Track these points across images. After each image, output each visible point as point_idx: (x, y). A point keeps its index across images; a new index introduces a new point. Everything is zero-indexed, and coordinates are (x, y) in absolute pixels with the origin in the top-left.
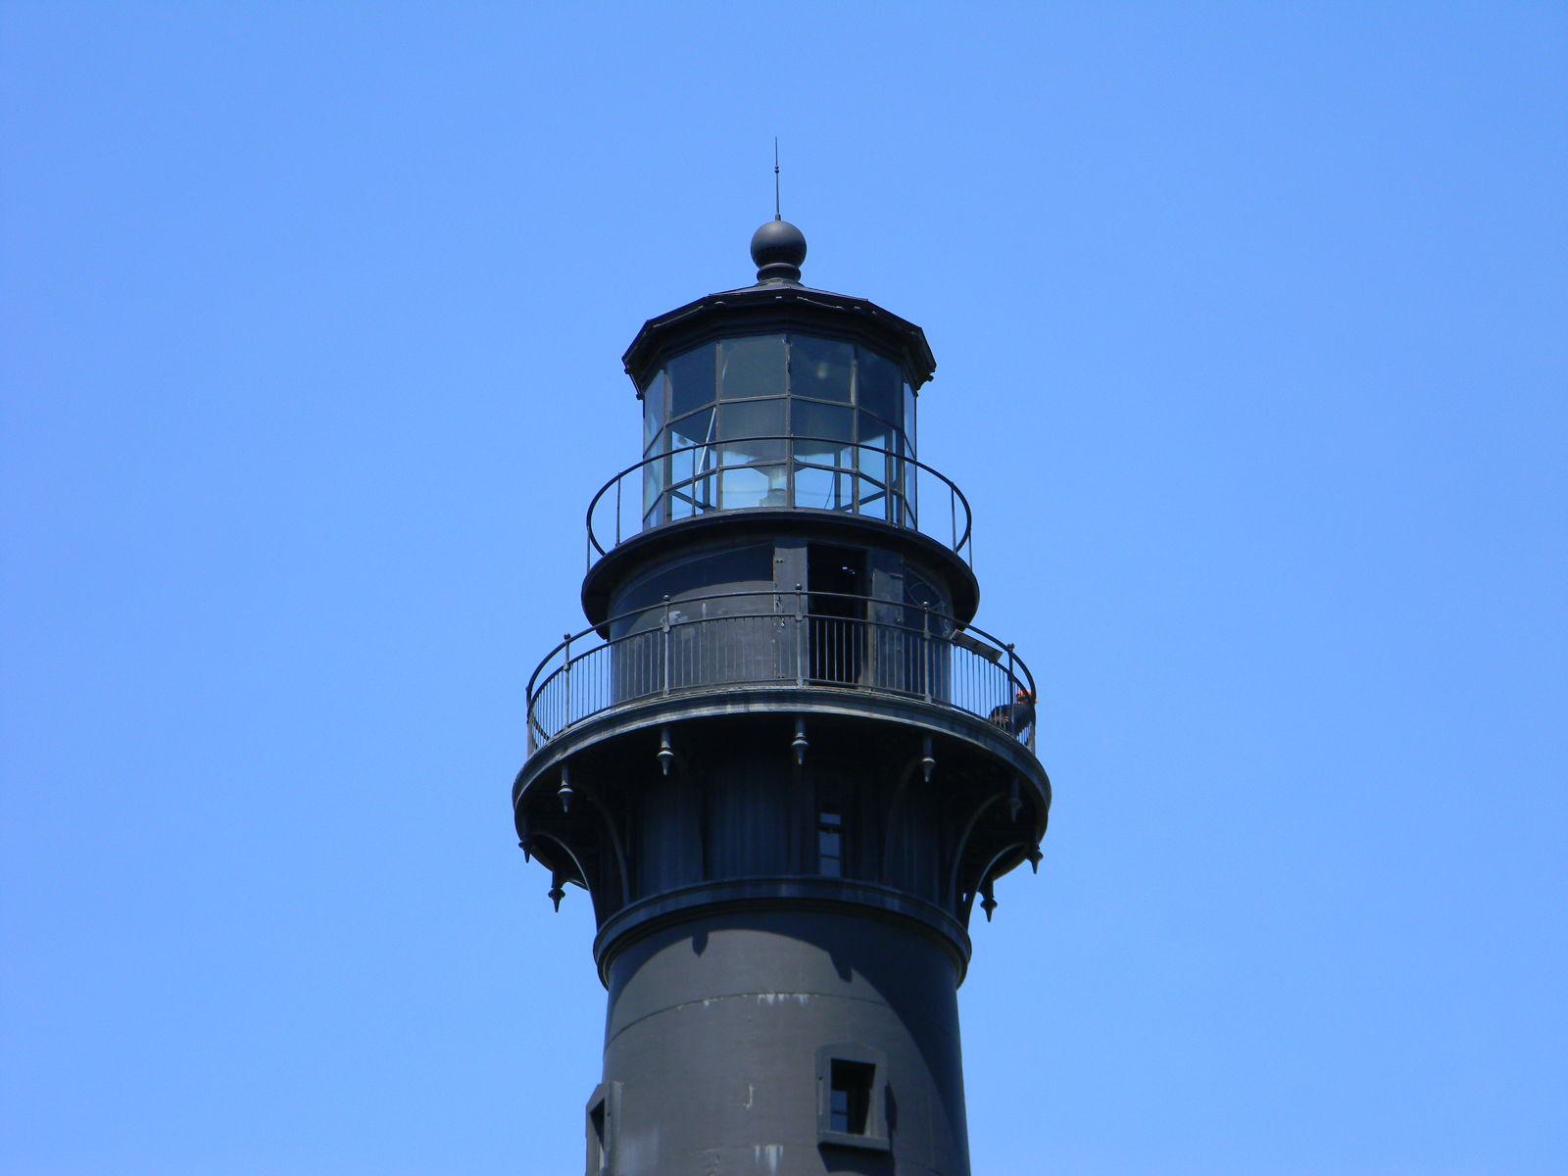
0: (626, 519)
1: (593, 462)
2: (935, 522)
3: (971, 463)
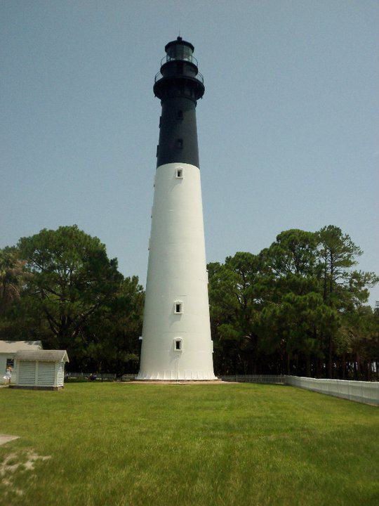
0: (165, 62)
1: (163, 58)
2: (195, 63)
3: (196, 58)
